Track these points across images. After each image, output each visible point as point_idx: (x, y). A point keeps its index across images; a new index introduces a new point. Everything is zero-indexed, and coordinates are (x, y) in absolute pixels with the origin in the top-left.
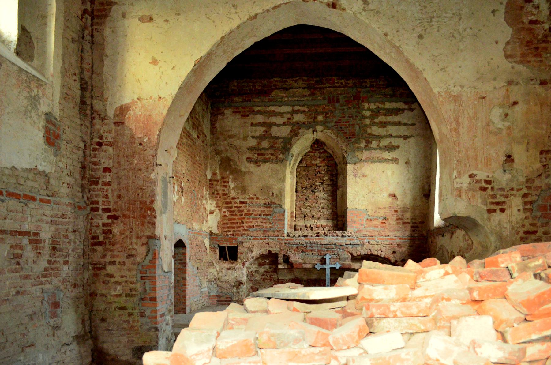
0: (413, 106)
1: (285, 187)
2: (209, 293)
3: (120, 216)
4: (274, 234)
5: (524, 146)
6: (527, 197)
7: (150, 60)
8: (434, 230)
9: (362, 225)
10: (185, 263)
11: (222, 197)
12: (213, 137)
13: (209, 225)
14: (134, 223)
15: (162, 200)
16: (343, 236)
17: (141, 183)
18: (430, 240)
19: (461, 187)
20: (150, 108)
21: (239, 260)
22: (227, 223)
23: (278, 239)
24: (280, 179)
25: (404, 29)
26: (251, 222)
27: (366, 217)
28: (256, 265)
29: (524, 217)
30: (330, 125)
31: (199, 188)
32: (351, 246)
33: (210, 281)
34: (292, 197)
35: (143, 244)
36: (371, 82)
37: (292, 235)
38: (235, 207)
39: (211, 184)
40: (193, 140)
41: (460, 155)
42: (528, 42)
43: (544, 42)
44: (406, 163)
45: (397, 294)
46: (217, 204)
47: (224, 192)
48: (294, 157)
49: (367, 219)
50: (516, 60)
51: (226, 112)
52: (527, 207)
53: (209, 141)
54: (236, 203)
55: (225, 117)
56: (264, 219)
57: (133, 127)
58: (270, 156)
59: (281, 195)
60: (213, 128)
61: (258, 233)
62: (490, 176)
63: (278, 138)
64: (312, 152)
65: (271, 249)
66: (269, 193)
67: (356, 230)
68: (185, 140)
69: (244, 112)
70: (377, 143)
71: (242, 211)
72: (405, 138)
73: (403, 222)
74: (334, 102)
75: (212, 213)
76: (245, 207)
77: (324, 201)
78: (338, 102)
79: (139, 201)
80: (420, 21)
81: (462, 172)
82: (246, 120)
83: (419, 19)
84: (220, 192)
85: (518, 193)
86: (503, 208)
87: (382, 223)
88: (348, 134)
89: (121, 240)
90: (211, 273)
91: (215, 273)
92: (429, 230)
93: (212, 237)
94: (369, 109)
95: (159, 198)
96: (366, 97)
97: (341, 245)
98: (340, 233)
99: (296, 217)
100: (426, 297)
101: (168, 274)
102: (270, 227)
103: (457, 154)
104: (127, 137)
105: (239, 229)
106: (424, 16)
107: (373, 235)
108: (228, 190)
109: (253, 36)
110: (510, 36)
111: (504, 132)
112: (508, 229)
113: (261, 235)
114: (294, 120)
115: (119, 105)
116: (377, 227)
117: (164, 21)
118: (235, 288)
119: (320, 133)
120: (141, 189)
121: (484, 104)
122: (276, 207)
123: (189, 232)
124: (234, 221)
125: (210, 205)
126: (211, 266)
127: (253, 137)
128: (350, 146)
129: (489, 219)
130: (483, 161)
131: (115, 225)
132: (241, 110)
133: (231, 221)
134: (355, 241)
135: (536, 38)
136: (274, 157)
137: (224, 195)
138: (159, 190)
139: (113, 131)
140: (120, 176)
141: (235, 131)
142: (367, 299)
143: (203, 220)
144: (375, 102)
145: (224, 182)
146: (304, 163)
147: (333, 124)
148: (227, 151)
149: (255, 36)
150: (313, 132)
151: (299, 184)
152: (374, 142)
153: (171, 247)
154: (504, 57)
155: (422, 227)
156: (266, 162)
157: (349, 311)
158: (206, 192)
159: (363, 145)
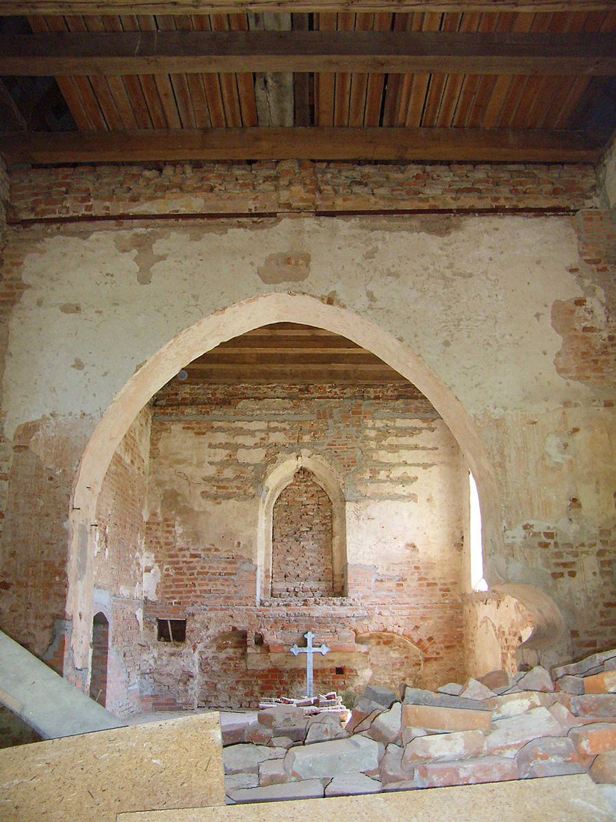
0: (433, 425)
1: (257, 534)
2: (141, 692)
3: (12, 584)
4: (241, 601)
5: (593, 486)
6: (604, 556)
7: (73, 363)
8: (472, 594)
9: (369, 588)
10: (107, 648)
11: (164, 547)
12: (154, 462)
13: (144, 589)
14: (33, 594)
15: (77, 561)
16: (342, 604)
17: (48, 534)
18: (466, 608)
19: (514, 543)
20: (67, 427)
21: (188, 641)
22: (171, 586)
23: (247, 609)
24: (250, 523)
25: (424, 333)
26: (207, 585)
27: (375, 576)
28: (214, 649)
29: (602, 583)
30: (320, 448)
31: (131, 535)
32: (354, 619)
33: (143, 674)
34: (267, 548)
35: (45, 627)
36: (375, 392)
37: (266, 604)
38: (183, 562)
39: (149, 528)
40: (123, 466)
41: (509, 499)
42: (584, 353)
43: (603, 353)
44: (428, 500)
45: (465, 748)
46: (156, 557)
47: (168, 541)
48: (270, 492)
49: (377, 580)
50: (570, 375)
51: (173, 427)
52: (604, 569)
53: (148, 469)
54: (184, 556)
55: (172, 434)
56: (226, 580)
57: (42, 455)
58: (235, 490)
59: (251, 546)
60: (154, 449)
61: (217, 600)
62: (552, 526)
63: (248, 465)
64: (296, 485)
65: (236, 625)
66: (233, 544)
67: (361, 595)
68: (113, 468)
69: (200, 428)
70: (387, 473)
71: (194, 568)
72: (425, 466)
73: (427, 583)
74: (325, 417)
75: (148, 570)
76: (198, 562)
77: (313, 554)
78: (331, 416)
79: (44, 561)
80: (444, 324)
81: (513, 522)
82: (203, 440)
83: (443, 322)
84: (162, 541)
85: (591, 550)
86: (573, 572)
87: (398, 585)
88: (346, 461)
89: (11, 620)
90: (145, 661)
91: (151, 661)
92: (463, 595)
93: (148, 607)
94: (373, 428)
95: (73, 558)
96: (369, 412)
97: (340, 618)
98: (337, 600)
99: (272, 578)
100: (508, 747)
101: (82, 672)
102: (236, 592)
103: (504, 497)
104: (31, 468)
105: (188, 595)
106: (450, 319)
107: (385, 602)
108: (174, 537)
109: (219, 335)
110: (561, 346)
111: (565, 468)
112: (582, 600)
113: (222, 603)
114: (270, 441)
115: (24, 422)
116: (391, 591)
117: (96, 312)
118: (181, 684)
119: (305, 462)
120: (48, 543)
121: (535, 431)
122: (244, 563)
123: (114, 601)
124: (181, 583)
125: (146, 559)
126: (145, 650)
127: (211, 463)
128: (349, 477)
129: (555, 586)
130: (541, 507)
131: (4, 597)
132: (194, 425)
133: (176, 583)
134: (361, 612)
135: (593, 349)
136: (241, 492)
137: (167, 544)
138: (74, 545)
139: (11, 459)
140: (16, 524)
141: (185, 454)
142: (422, 757)
143: (135, 581)
144: (381, 419)
145: (168, 526)
146: (284, 502)
147: (324, 447)
148: (172, 481)
149: (222, 335)
150: (297, 457)
151: (278, 530)
152: (382, 472)
153: (89, 631)
154: (556, 373)
155: (454, 589)
156: (229, 498)
157: (391, 773)
158: (141, 541)
159: (367, 476)
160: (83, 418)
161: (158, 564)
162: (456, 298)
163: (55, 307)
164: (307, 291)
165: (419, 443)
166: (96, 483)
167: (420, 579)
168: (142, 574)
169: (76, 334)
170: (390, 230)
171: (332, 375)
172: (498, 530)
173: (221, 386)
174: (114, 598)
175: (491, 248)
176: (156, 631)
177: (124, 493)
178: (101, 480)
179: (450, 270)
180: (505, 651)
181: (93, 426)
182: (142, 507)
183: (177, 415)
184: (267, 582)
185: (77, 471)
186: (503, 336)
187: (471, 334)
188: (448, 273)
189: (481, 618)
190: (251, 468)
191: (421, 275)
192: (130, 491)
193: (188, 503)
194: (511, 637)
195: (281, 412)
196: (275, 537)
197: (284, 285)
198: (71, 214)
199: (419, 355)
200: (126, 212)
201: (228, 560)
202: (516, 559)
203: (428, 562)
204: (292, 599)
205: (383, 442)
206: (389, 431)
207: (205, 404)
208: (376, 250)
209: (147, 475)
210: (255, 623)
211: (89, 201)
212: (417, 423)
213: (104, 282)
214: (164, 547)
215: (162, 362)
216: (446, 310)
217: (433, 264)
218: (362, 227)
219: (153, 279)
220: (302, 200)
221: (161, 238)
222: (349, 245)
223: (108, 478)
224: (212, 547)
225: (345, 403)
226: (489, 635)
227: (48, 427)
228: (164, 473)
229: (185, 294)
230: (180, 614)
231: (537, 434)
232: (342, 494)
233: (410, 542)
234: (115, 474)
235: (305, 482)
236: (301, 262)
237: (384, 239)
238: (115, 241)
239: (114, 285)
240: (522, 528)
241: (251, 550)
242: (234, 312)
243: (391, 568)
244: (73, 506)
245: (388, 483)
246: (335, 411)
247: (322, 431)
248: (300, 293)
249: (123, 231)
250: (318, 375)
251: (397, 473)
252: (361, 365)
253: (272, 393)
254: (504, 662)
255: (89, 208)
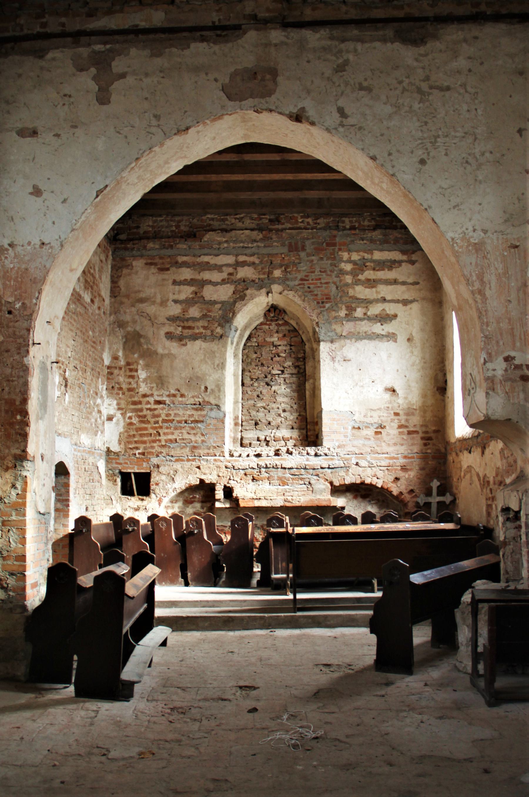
0: (414, 257)
7: (31, 190)
8: (455, 442)
11: (127, 393)
16: (316, 455)
17: (8, 371)
18: (450, 458)
20: (27, 258)
21: (153, 495)
22: (134, 436)
23: (215, 460)
24: (218, 365)
25: (398, 151)
27: (352, 424)
31: (92, 380)
34: (236, 394)
36: (351, 222)
37: (236, 454)
38: (147, 409)
41: (489, 329)
44: (409, 340)
46: (118, 404)
47: (130, 386)
48: (239, 332)
49: (354, 428)
51: (134, 263)
54: (148, 403)
55: (133, 271)
56: (193, 428)
58: (202, 330)
59: (219, 390)
60: (115, 287)
63: (215, 302)
65: (203, 477)
66: (200, 388)
67: (337, 444)
68: (72, 306)
70: (364, 310)
71: (159, 416)
72: (405, 303)
74: (297, 249)
76: (163, 409)
78: (303, 249)
80: (420, 141)
81: (493, 353)
83: (419, 139)
84: (124, 386)
87: (377, 433)
93: (110, 458)
94: (349, 261)
96: (344, 244)
98: (311, 450)
99: (242, 425)
102: (203, 441)
103: (485, 327)
108: (137, 382)
109: (182, 158)
113: (189, 454)
116: (369, 439)
122: (211, 409)
123: (75, 450)
127: (176, 301)
132: (157, 260)
136: (209, 332)
137: (130, 390)
138: (34, 382)
141: (148, 292)
147: (297, 282)
149: (185, 157)
150: (268, 293)
151: (247, 373)
152: (359, 310)
158: (102, 387)
160: (42, 248)
161: (120, 412)
162: (432, 113)
163: (11, 131)
164: (274, 108)
165: (398, 278)
166: (56, 317)
167: (400, 427)
168: (103, 423)
169: (34, 159)
170: (363, 41)
171: (304, 203)
172: (478, 363)
173: (185, 218)
174: (75, 447)
175: (469, 58)
176: (119, 484)
177: (84, 334)
178: (61, 314)
179: (427, 82)
180: (490, 502)
181: (53, 257)
182: (103, 350)
183: (139, 250)
184: (236, 431)
185: (36, 304)
186: (483, 154)
187: (448, 152)
188: (424, 86)
189: (465, 466)
190: (218, 306)
191: (396, 89)
192: (91, 333)
193: (151, 345)
194: (496, 486)
195: (250, 245)
196: (245, 382)
197: (250, 102)
198: (26, 31)
199: (393, 175)
200: (83, 28)
201: (194, 406)
202: (497, 393)
203: (409, 408)
204: (263, 449)
205: (360, 277)
206: (367, 264)
207: (169, 237)
208: (346, 62)
209: (108, 315)
210: (224, 475)
211: (44, 17)
212: (396, 255)
213: (61, 104)
214: (127, 393)
215: (123, 187)
216: (422, 126)
217: (408, 77)
218: (332, 38)
219: (113, 98)
220: (268, 10)
221: (120, 55)
222: (319, 58)
223: (67, 318)
224: (177, 392)
225: (319, 234)
226: (473, 485)
227: (6, 258)
228: (125, 313)
229: (146, 114)
230: (144, 466)
231: (520, 259)
232: (315, 332)
233: (389, 386)
234: (74, 313)
235: (277, 320)
236: (268, 77)
237: (356, 50)
238: (72, 59)
239: (72, 106)
240: (503, 361)
241: (219, 396)
242: (198, 132)
243: (369, 415)
244: (33, 340)
245: (366, 321)
246: (307, 243)
247: (295, 265)
248: (266, 110)
249: (80, 49)
250: (289, 204)
251: (375, 310)
252: (334, 192)
253: (240, 225)
254: (489, 514)
255: (44, 25)
